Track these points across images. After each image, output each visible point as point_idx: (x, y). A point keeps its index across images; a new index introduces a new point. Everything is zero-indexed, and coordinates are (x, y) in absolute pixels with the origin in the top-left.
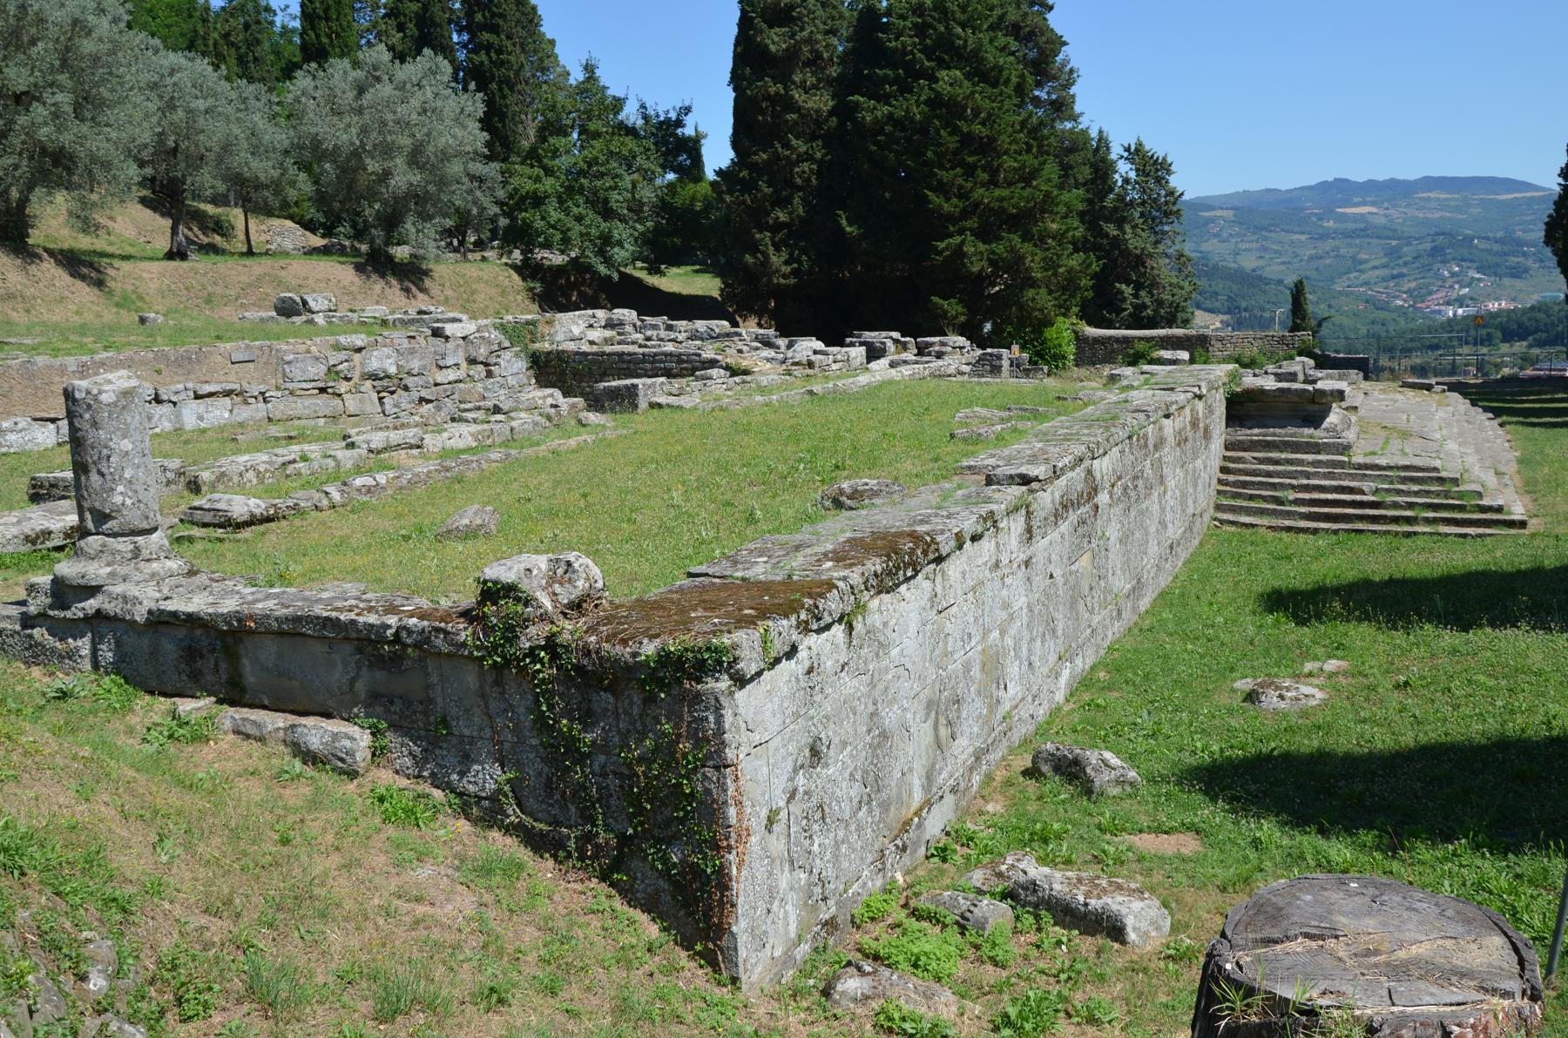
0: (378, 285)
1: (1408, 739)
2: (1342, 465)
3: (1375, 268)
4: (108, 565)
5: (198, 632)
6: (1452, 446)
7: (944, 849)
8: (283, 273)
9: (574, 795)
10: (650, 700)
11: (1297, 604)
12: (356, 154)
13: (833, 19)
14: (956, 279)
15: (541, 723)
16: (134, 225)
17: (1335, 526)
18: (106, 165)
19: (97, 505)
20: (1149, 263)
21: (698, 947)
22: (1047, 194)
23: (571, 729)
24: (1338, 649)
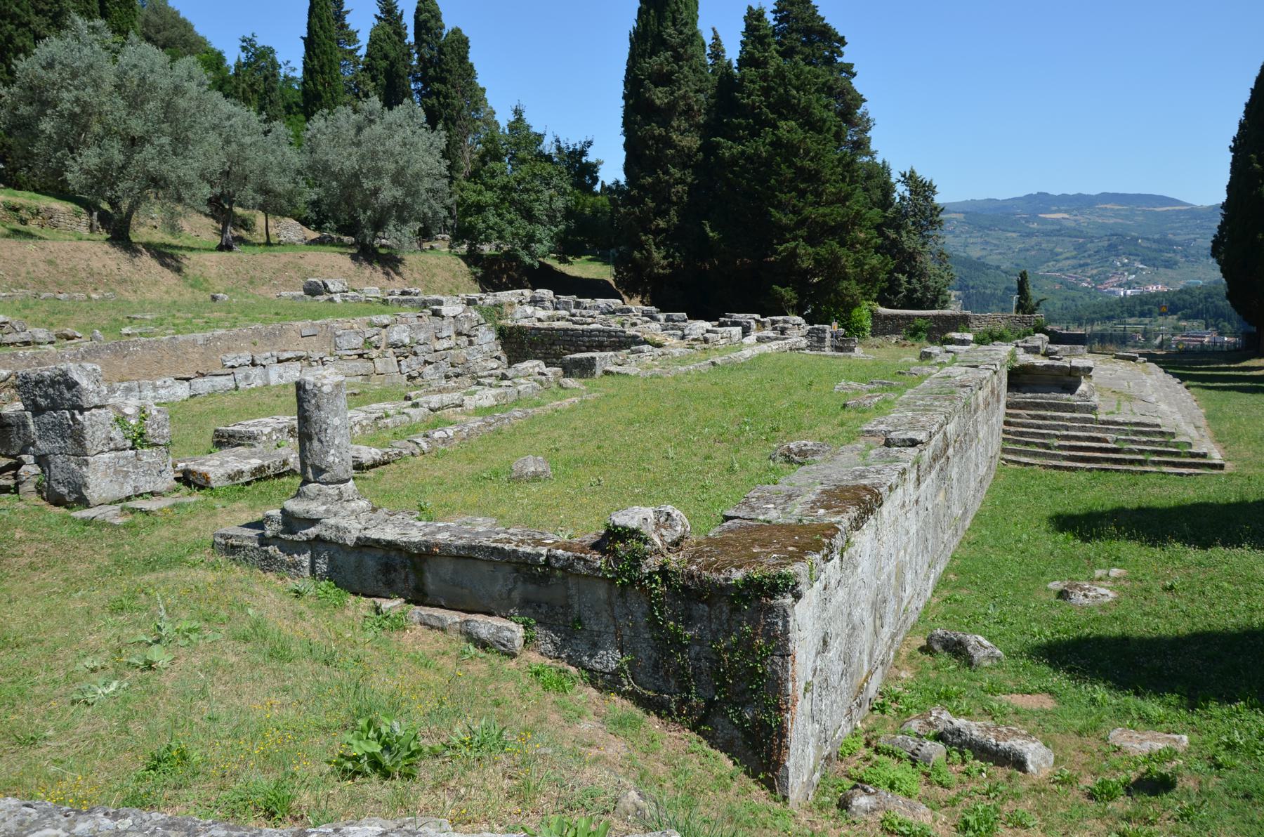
0: (367, 270)
1: (1184, 628)
2: (1091, 421)
3: (1067, 258)
4: (323, 504)
5: (393, 553)
6: (1163, 407)
7: (883, 705)
8: (301, 261)
9: (674, 672)
10: (736, 609)
11: (1081, 525)
12: (356, 175)
13: (701, 81)
14: (789, 272)
15: (654, 624)
16: (199, 228)
17: (1089, 466)
18: (189, 186)
19: (317, 462)
20: (918, 259)
21: (761, 776)
22: (858, 212)
23: (676, 628)
24: (1116, 560)
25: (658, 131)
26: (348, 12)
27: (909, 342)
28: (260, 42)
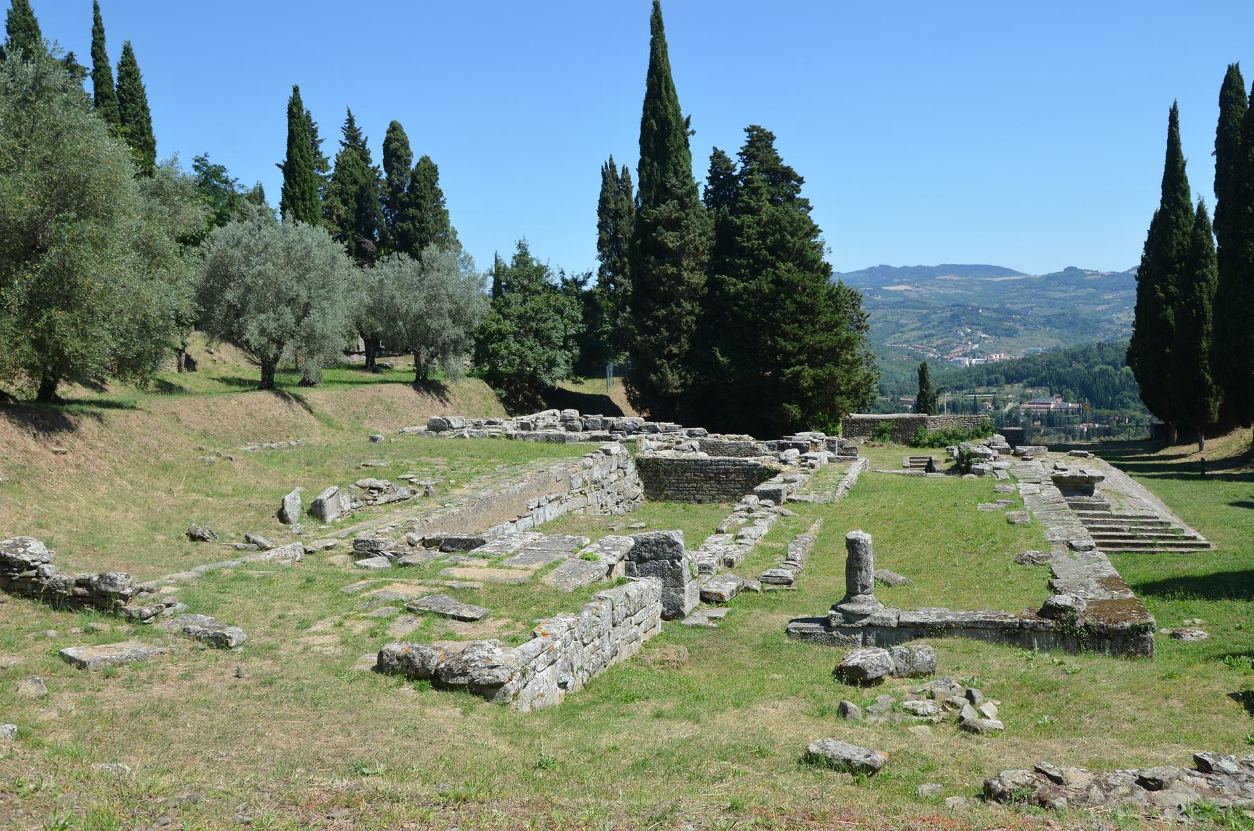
2: (1108, 516)
25: (671, 270)
26: (321, 141)
27: (877, 443)
28: (212, 161)
